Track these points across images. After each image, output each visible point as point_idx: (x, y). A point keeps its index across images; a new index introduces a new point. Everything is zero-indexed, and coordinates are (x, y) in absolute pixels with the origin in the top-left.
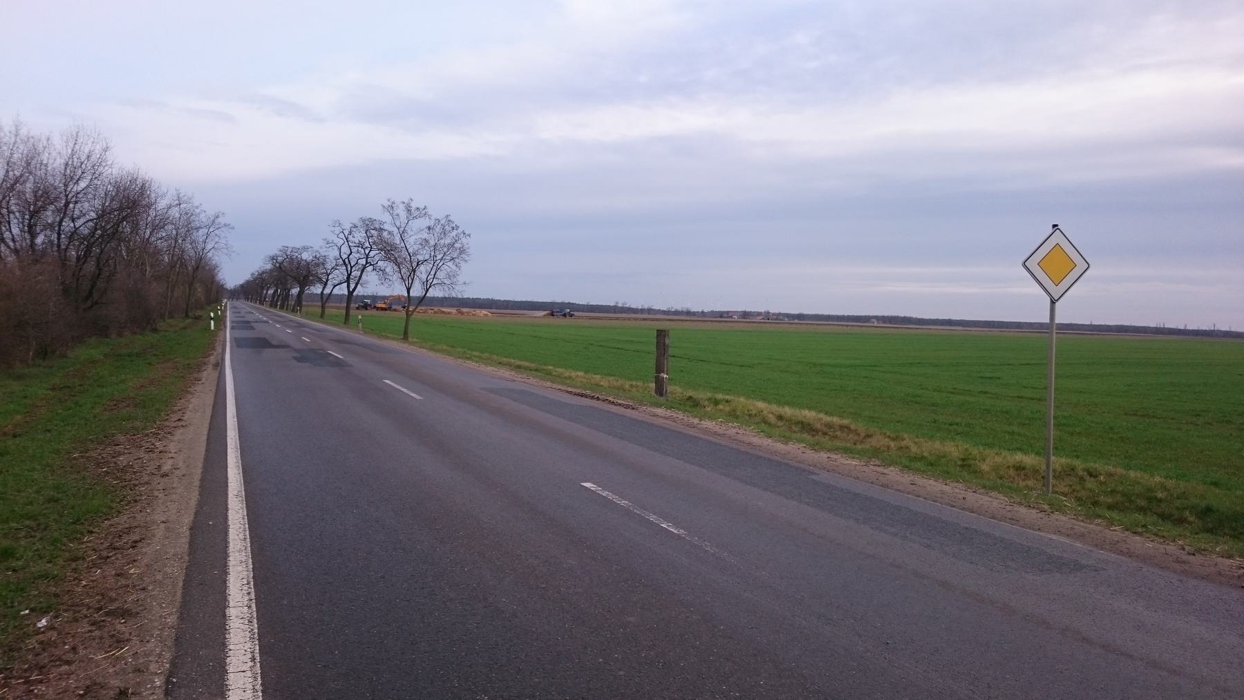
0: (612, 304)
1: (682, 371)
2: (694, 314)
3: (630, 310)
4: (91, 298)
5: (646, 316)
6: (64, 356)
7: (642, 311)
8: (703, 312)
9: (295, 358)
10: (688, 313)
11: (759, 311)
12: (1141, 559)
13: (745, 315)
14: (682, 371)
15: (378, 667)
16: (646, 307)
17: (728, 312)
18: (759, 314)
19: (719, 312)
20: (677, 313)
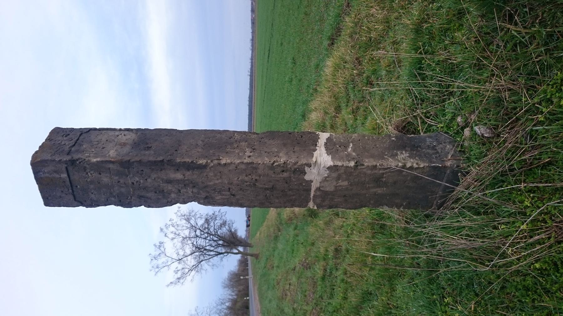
0: (249, 77)
1: (282, 44)
2: (253, 37)
3: (252, 66)
4: (317, 165)
5: (254, 61)
6: (279, 240)
7: (252, 63)
8: (252, 33)
9: (61, 160)
10: (252, 40)
11: (250, 4)
12: (287, 222)
13: (253, 11)
14: (282, 44)
15: (388, 302)
16: (250, 61)
17: (252, 20)
18: (252, 4)
19: (252, 24)
20: (252, 46)
